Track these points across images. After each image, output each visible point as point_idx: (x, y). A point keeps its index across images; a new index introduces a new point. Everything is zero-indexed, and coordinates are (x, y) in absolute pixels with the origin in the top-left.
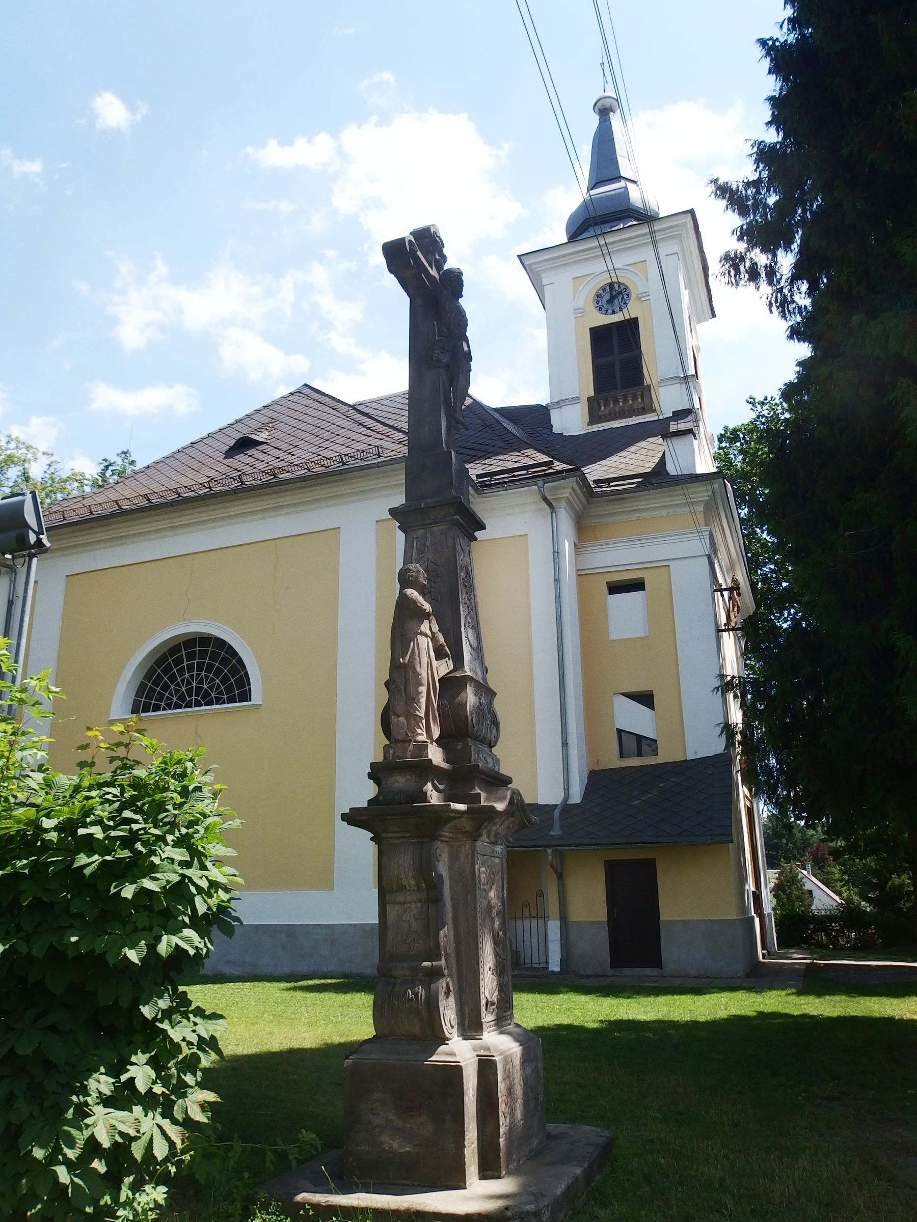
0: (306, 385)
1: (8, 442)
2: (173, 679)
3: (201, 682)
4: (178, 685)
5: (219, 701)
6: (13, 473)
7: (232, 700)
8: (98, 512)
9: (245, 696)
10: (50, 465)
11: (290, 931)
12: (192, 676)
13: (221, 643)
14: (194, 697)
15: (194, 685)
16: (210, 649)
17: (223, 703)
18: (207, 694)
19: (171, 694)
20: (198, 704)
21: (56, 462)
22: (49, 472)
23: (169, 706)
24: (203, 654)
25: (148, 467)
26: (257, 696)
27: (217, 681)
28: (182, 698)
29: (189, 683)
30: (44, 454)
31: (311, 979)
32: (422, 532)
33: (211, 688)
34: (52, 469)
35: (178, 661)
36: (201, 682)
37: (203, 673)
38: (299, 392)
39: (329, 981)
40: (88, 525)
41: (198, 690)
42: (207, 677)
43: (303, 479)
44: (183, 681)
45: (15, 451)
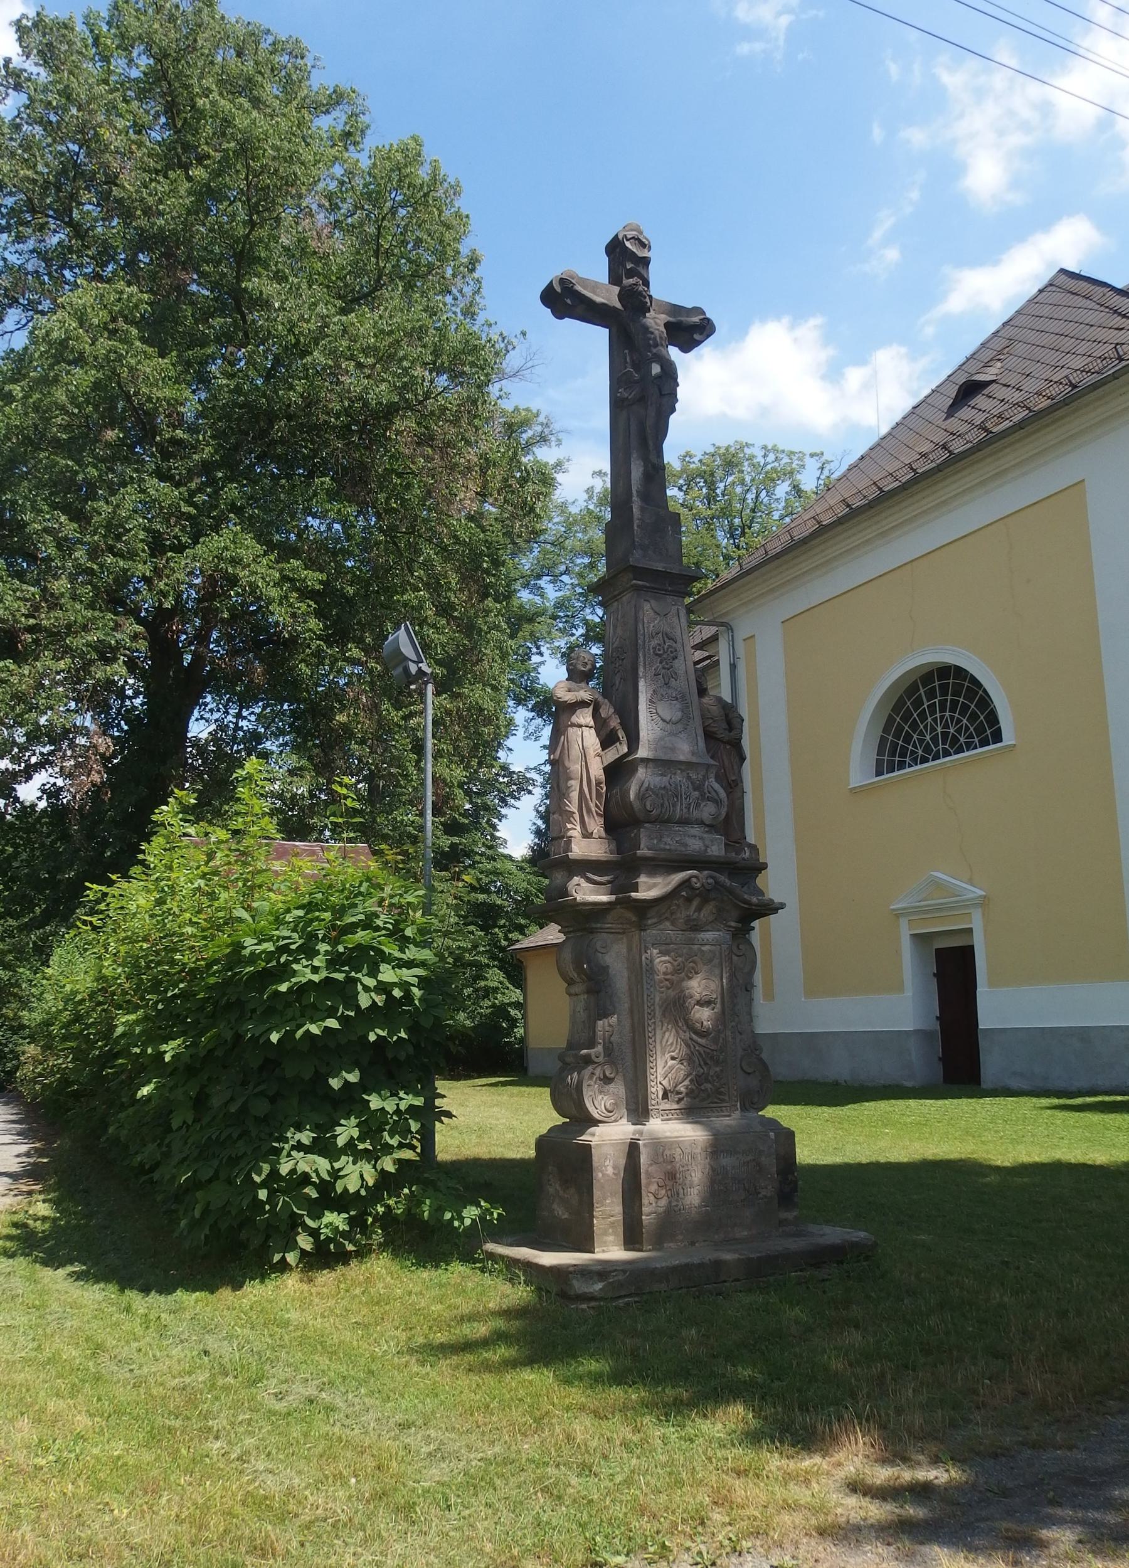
0: (1063, 271)
1: (765, 456)
2: (914, 726)
3: (946, 726)
4: (921, 734)
5: (970, 746)
6: (782, 489)
7: (984, 743)
8: (798, 534)
9: (997, 737)
10: (822, 468)
11: (1083, 1034)
12: (935, 720)
13: (960, 672)
14: (941, 746)
15: (939, 730)
16: (937, 683)
17: (975, 748)
18: (955, 740)
19: (915, 746)
20: (947, 754)
21: (828, 462)
22: (823, 477)
23: (915, 761)
24: (944, 689)
25: (862, 457)
26: (1009, 735)
27: (965, 721)
28: (927, 750)
29: (933, 729)
30: (812, 455)
31: (1089, 1096)
32: (616, 604)
33: (959, 731)
34: (826, 472)
35: (918, 703)
36: (946, 726)
37: (947, 714)
38: (1051, 285)
39: (1119, 1098)
40: (790, 555)
41: (945, 735)
42: (952, 718)
43: (1020, 425)
44: (926, 727)
45: (776, 464)
